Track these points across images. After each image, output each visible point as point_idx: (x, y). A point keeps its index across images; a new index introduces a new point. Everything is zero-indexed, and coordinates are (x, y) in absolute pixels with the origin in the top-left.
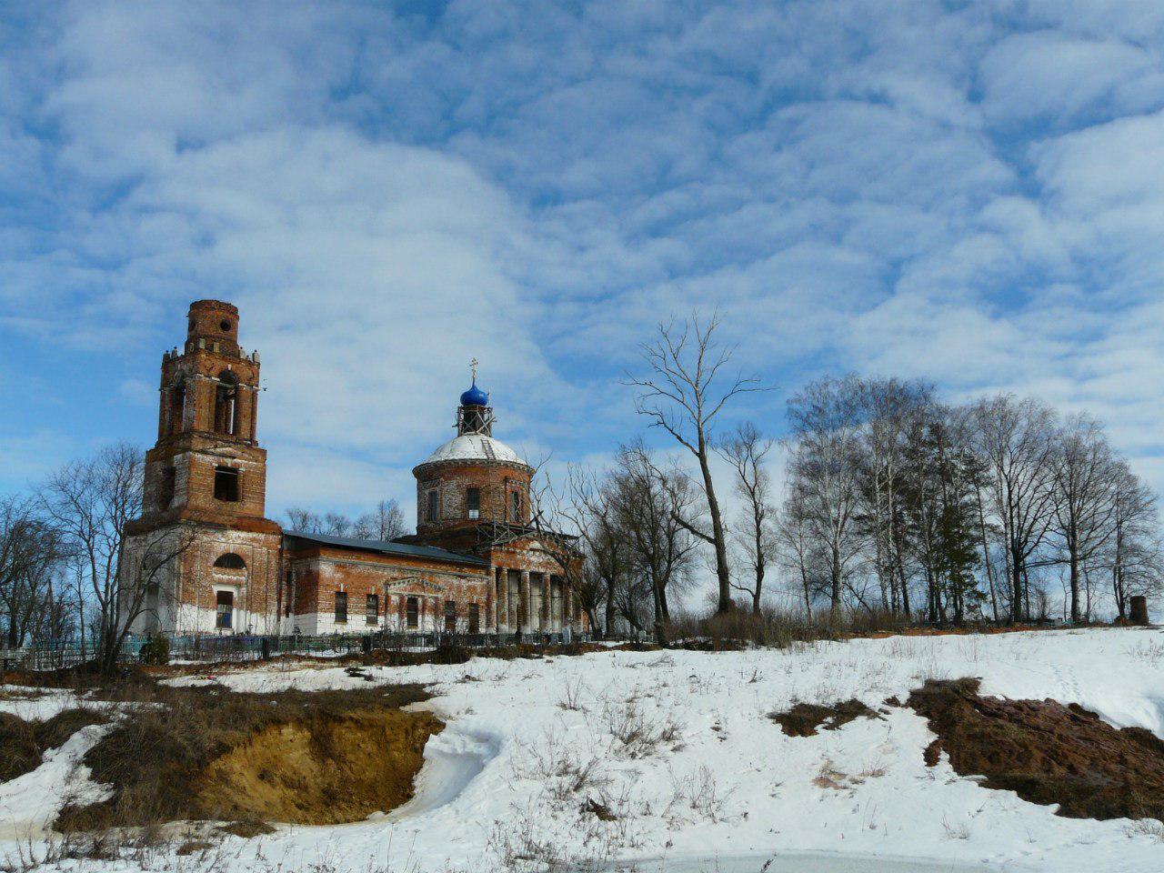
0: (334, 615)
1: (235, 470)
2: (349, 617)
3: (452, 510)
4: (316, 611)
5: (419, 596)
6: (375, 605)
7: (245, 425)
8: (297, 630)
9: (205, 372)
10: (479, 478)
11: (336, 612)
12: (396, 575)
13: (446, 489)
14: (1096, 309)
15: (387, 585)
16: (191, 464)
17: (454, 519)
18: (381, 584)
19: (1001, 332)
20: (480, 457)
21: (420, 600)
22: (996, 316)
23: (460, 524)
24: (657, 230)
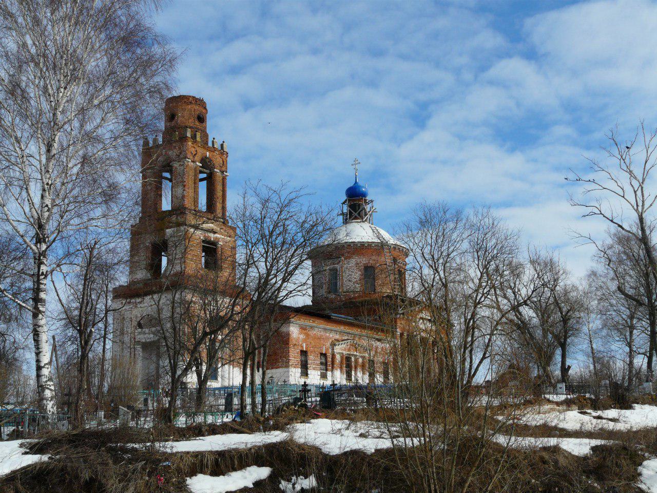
0: (299, 370)
1: (214, 243)
2: (309, 372)
3: (352, 284)
4: (287, 366)
5: (353, 355)
6: (327, 364)
7: (219, 206)
8: (305, 382)
9: (191, 157)
10: (374, 258)
11: (301, 368)
12: (337, 337)
13: (345, 266)
14: (588, 147)
15: (333, 345)
16: (186, 237)
17: (354, 292)
18: (328, 344)
19: (515, 162)
20: (373, 241)
21: (353, 359)
22: (512, 150)
23: (359, 297)
24: (235, 70)
